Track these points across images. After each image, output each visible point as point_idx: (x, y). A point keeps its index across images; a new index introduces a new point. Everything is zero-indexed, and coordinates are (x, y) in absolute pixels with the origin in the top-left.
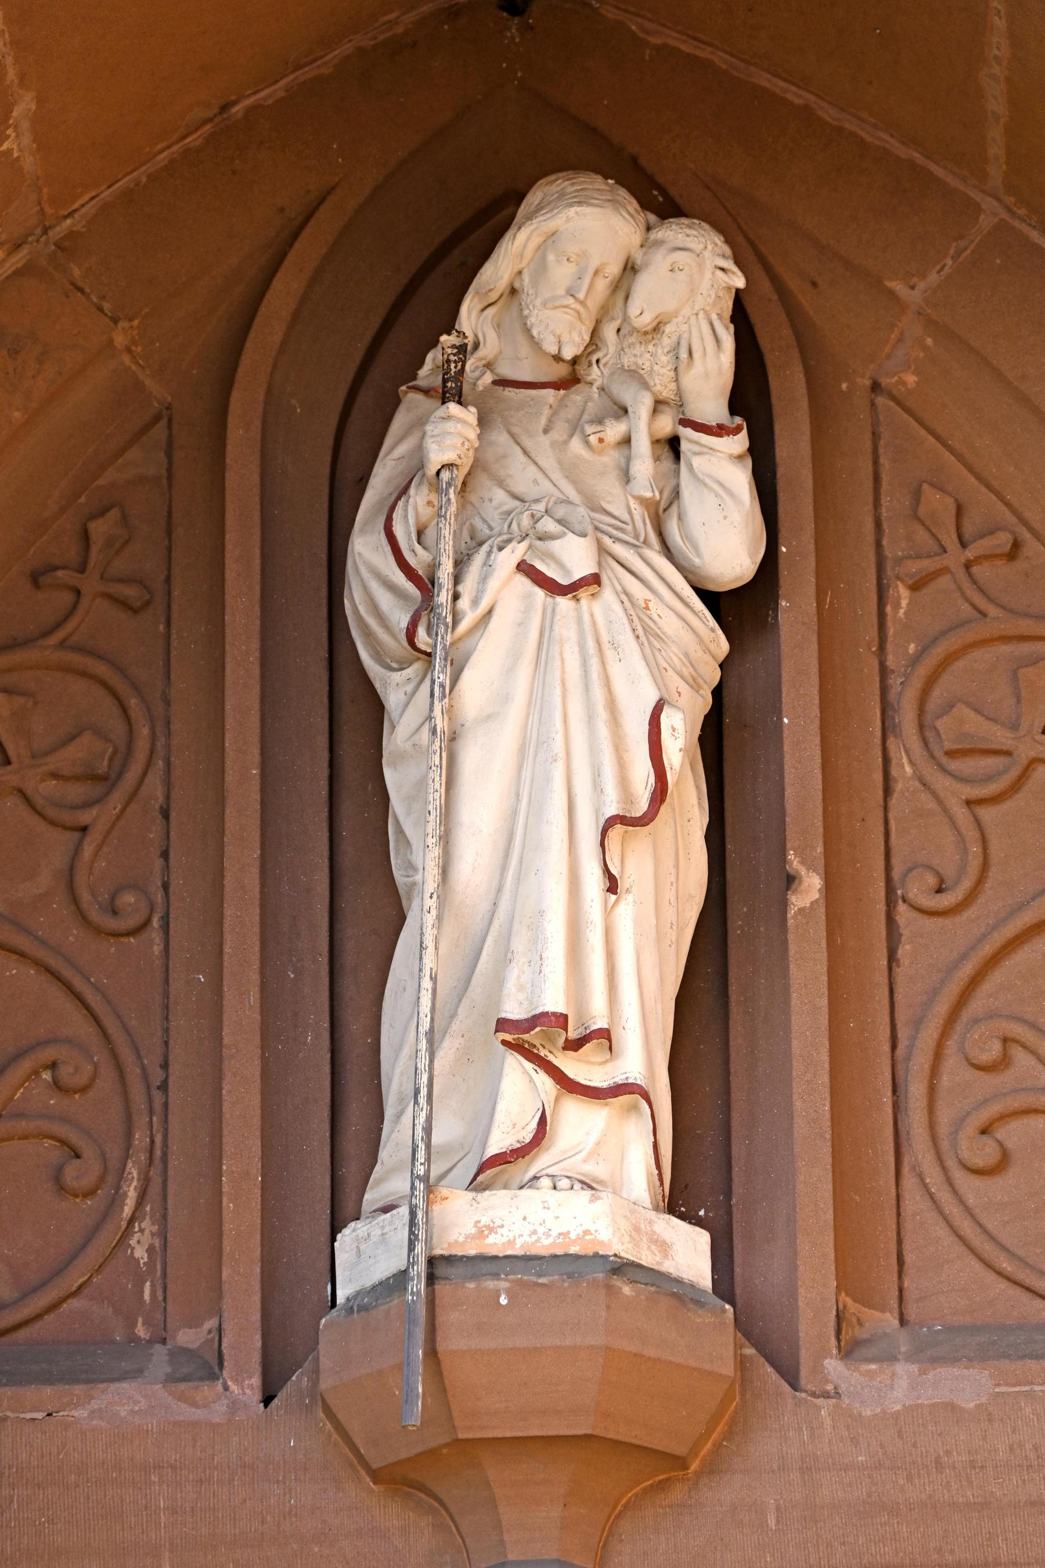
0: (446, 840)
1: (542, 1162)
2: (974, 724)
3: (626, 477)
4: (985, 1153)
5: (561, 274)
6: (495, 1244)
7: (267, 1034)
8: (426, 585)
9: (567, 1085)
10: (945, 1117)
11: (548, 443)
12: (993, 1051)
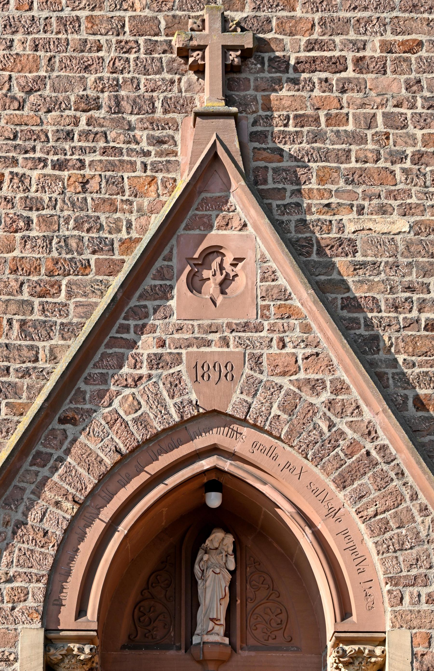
0: (205, 600)
1: (213, 631)
2: (255, 583)
3: (222, 560)
4: (255, 628)
5: (217, 539)
6: (209, 641)
7: (186, 614)
8: (203, 571)
9: (216, 624)
10: (251, 624)
11: (166, 74)
12: (256, 618)
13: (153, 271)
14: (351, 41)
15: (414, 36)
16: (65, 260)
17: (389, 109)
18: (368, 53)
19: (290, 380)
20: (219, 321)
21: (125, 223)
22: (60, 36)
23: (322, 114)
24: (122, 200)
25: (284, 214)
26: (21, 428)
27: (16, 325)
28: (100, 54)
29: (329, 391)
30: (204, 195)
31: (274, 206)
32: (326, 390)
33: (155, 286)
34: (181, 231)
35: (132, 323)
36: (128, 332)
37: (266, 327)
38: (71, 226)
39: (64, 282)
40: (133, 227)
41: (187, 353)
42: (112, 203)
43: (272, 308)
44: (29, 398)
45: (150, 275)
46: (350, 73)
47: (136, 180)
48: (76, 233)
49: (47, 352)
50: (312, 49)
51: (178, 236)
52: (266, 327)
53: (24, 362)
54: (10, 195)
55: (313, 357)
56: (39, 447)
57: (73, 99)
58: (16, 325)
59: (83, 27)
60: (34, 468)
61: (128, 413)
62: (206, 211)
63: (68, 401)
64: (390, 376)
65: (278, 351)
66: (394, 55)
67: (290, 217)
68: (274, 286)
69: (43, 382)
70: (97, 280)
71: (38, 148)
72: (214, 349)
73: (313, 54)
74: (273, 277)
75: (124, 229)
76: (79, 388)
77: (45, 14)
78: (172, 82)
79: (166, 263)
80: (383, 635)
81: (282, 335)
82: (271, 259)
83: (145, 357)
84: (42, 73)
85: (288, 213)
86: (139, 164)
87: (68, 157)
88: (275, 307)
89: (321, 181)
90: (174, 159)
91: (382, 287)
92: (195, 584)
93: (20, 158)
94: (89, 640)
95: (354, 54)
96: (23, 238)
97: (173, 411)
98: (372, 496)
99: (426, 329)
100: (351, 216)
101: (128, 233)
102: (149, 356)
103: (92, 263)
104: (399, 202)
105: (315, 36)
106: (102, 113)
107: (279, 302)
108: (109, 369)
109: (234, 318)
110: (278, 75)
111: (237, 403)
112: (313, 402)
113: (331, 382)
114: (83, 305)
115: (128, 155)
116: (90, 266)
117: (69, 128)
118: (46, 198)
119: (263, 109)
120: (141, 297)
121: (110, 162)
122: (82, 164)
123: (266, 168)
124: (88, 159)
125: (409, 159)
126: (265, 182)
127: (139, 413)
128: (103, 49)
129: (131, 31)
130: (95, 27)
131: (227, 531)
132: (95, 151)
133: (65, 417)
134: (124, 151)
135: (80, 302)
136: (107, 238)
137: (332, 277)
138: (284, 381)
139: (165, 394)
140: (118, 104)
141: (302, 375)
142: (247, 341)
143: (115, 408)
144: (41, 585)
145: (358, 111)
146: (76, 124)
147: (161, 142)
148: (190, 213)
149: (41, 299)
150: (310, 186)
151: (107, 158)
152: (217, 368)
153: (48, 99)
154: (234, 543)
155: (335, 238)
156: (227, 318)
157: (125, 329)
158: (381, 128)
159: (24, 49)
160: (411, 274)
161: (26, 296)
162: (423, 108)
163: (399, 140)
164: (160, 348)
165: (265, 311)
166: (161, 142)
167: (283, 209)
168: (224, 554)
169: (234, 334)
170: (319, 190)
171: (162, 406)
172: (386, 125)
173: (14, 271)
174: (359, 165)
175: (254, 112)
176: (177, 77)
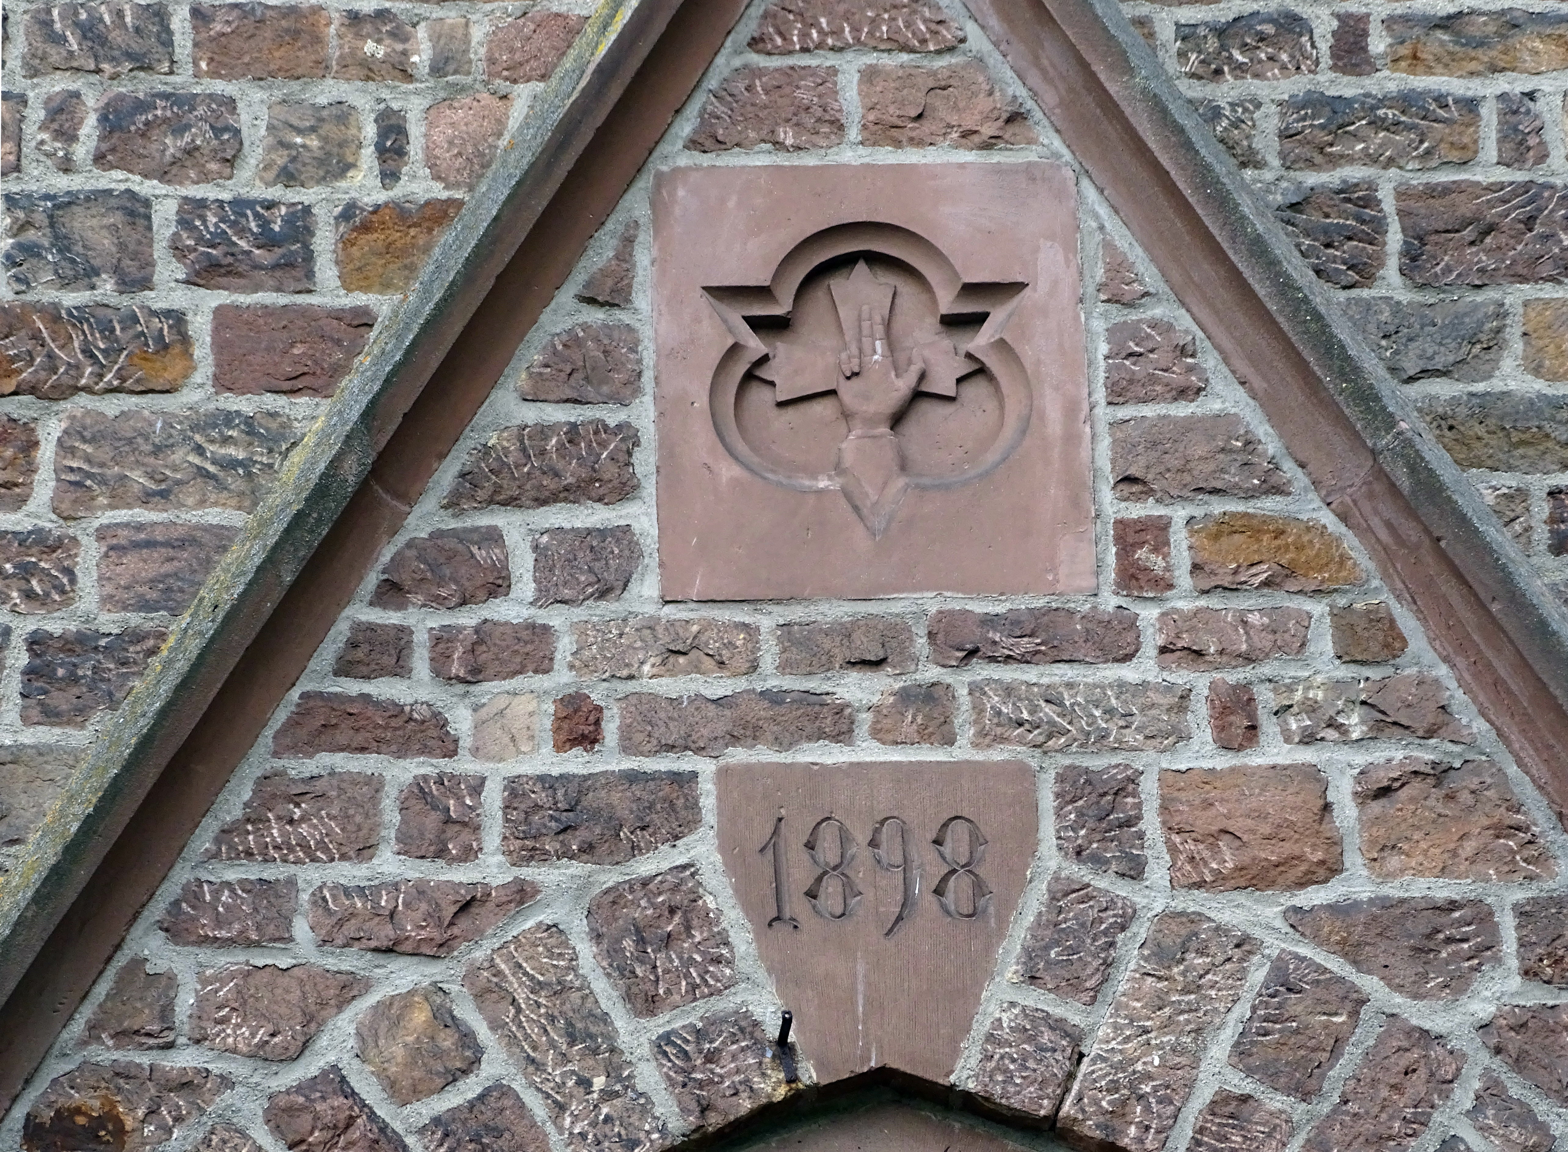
16: (53, 314)
19: (1297, 910)
20: (896, 608)
21: (370, 131)
25: (1218, 72)
29: (1513, 963)
31: (1166, 32)
32: (1498, 961)
33: (543, 431)
37: (1152, 640)
38: (82, 151)
40: (415, 148)
41: (724, 775)
43: (1179, 537)
51: (659, 175)
52: (1152, 640)
55: (1415, 788)
62: (805, 50)
63: (78, 1027)
65: (1223, 761)
67: (1252, 86)
68: (1189, 425)
70: (229, 418)
74: (1176, 377)
75: (368, 155)
76: (138, 963)
79: (596, 316)
81: (1234, 677)
82: (1162, 287)
85: (1240, 69)
88: (1192, 533)
101: (389, 177)
107: (1218, 507)
108: (298, 862)
111: (1005, 1033)
112: (1436, 1023)
113: (1523, 914)
114: (150, 544)
116: (185, 340)
135: (140, 527)
136: (270, 205)
137: (1496, 385)
142: (1048, 709)
143: (335, 1068)
148: (720, 60)
152: (891, 852)
155: (1501, 186)
156: (939, 587)
164: (577, 751)
165: (1141, 554)
167: (1212, 44)
169: (981, 671)
171: (595, 1052)
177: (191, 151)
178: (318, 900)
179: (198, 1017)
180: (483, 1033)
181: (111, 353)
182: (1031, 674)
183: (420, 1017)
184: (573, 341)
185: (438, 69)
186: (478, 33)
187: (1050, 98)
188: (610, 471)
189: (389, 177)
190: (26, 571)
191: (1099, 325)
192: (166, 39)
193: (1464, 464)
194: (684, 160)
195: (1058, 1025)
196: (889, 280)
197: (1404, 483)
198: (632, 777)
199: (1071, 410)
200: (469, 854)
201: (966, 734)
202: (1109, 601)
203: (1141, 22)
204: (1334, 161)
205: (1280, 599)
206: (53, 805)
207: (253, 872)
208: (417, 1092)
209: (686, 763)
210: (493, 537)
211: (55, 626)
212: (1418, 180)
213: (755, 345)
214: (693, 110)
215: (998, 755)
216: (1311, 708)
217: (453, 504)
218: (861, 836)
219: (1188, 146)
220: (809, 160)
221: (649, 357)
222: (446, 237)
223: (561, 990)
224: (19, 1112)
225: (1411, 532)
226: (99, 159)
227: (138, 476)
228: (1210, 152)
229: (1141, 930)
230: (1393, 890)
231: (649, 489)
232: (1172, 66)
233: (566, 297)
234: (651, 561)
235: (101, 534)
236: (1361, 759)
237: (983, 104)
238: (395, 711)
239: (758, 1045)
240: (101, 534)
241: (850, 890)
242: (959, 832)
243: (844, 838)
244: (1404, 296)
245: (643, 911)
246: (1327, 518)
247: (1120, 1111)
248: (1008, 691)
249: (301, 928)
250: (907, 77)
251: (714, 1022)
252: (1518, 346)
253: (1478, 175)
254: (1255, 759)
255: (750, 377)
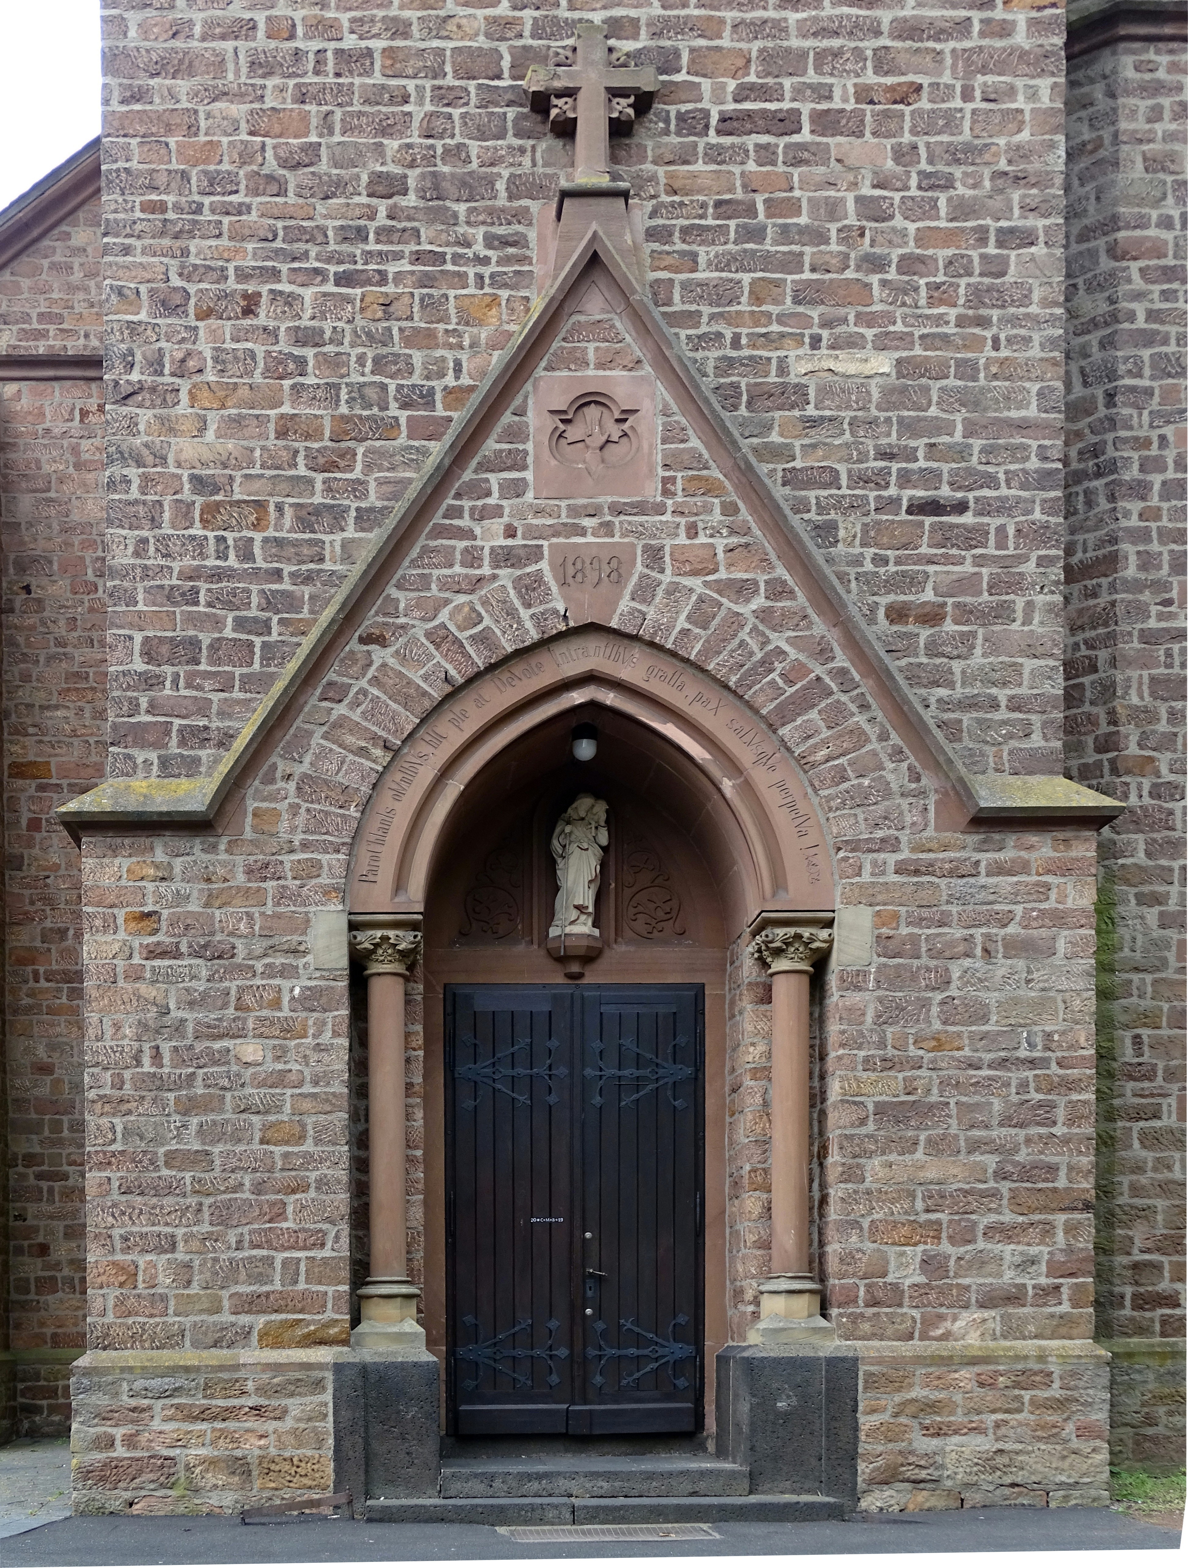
13: (498, 429)
14: (810, 86)
15: (910, 78)
16: (360, 417)
17: (867, 191)
18: (836, 104)
21: (451, 365)
22: (340, 80)
23: (760, 200)
24: (447, 331)
26: (302, 653)
27: (289, 512)
28: (407, 108)
30: (576, 318)
33: (501, 451)
34: (540, 372)
35: (467, 504)
36: (461, 517)
37: (670, 509)
38: (367, 370)
39: (360, 451)
40: (465, 370)
41: (550, 545)
42: (430, 334)
43: (679, 482)
44: (311, 612)
45: (494, 436)
46: (805, 135)
47: (467, 301)
48: (377, 378)
49: (338, 549)
50: (746, 99)
52: (670, 509)
53: (304, 562)
54: (272, 324)
56: (332, 676)
57: (365, 178)
58: (289, 512)
59: (377, 66)
60: (325, 704)
61: (461, 629)
63: (372, 612)
64: (852, 577)
65: (688, 542)
66: (878, 107)
67: (707, 353)
69: (333, 591)
70: (412, 447)
71: (312, 254)
72: (590, 539)
73: (747, 106)
75: (451, 372)
77: (315, 45)
78: (522, 150)
79: (517, 418)
80: (831, 915)
83: (487, 551)
84: (314, 139)
85: (703, 348)
86: (471, 276)
87: (359, 267)
89: (757, 298)
90: (526, 268)
91: (844, 453)
92: (554, 862)
93: (284, 268)
94: (413, 926)
95: (813, 105)
96: (293, 387)
97: (529, 624)
98: (823, 736)
99: (909, 512)
100: (800, 352)
101: (457, 378)
102: (492, 549)
103: (403, 421)
104: (875, 331)
105: (752, 78)
106: (411, 200)
107: (690, 473)
109: (623, 496)
110: (692, 138)
112: (740, 611)
113: (766, 582)
115: (454, 263)
116: (399, 425)
117: (362, 222)
118: (327, 326)
119: (667, 193)
120: (480, 467)
121: (426, 274)
122: (383, 278)
123: (671, 281)
124: (392, 269)
125: (894, 266)
126: (669, 302)
127: (480, 628)
128: (412, 99)
129: (455, 71)
130: (398, 65)
131: (597, 796)
132: (403, 257)
133: (370, 635)
134: (448, 257)
138: (695, 583)
139: (517, 603)
140: (436, 187)
141: (722, 574)
144: (341, 856)
145: (817, 194)
146: (372, 218)
147: (506, 243)
149: (326, 475)
150: (739, 308)
151: (422, 268)
152: (596, 565)
153: (325, 178)
154: (607, 811)
156: (612, 495)
157: (455, 512)
158: (852, 220)
159: (284, 101)
160: (889, 435)
161: (302, 470)
162: (920, 188)
163: (880, 239)
166: (506, 243)
168: (593, 825)
169: (622, 518)
170: (752, 313)
172: (859, 216)
173: (282, 434)
174: (815, 276)
175: (653, 197)
176: (531, 142)
177: (399, 370)
178: (438, 579)
179: (405, 609)
180: (483, 613)
181: (377, 428)
182: (636, 518)
183: (466, 609)
184: (510, 426)
185: (471, 346)
186: (483, 336)
187: (649, 356)
188: (520, 462)
189: (457, 378)
190: (354, 490)
191: (660, 422)
192: (391, 336)
193: (760, 461)
194: (543, 373)
195: (640, 611)
196: (600, 408)
197: (743, 466)
198: (525, 546)
199: (651, 446)
200: (480, 567)
201: (618, 535)
202: (659, 499)
203: (676, 334)
204: (729, 375)
205: (706, 498)
206: (364, 553)
207: (420, 571)
208: (466, 629)
209: (540, 542)
210: (487, 480)
211: (363, 505)
212: (752, 381)
213: (562, 427)
214: (546, 359)
215: (626, 540)
216: (713, 528)
217: (475, 471)
218: (588, 562)
219: (688, 370)
220: (579, 374)
221: (531, 430)
222: (474, 395)
223: (505, 602)
224: (357, 634)
225: (744, 480)
226: (372, 372)
227: (386, 464)
228: (693, 372)
229: (663, 586)
230: (732, 576)
231: (531, 467)
232: (684, 347)
233: (508, 413)
234: (531, 487)
235: (376, 479)
236: (725, 541)
237: (629, 358)
238: (459, 528)
239: (558, 616)
240: (376, 479)
241: (584, 576)
242: (615, 561)
243: (583, 562)
244: (746, 414)
245: (527, 581)
246: (721, 477)
247: (655, 633)
248: (630, 523)
249: (434, 586)
250: (607, 350)
251: (546, 610)
252: (777, 428)
253: (769, 380)
254: (696, 541)
255: (560, 436)
